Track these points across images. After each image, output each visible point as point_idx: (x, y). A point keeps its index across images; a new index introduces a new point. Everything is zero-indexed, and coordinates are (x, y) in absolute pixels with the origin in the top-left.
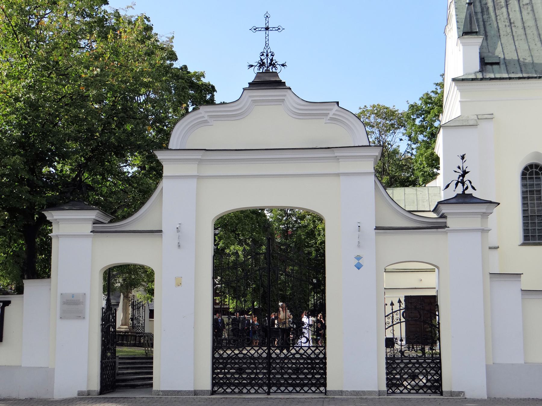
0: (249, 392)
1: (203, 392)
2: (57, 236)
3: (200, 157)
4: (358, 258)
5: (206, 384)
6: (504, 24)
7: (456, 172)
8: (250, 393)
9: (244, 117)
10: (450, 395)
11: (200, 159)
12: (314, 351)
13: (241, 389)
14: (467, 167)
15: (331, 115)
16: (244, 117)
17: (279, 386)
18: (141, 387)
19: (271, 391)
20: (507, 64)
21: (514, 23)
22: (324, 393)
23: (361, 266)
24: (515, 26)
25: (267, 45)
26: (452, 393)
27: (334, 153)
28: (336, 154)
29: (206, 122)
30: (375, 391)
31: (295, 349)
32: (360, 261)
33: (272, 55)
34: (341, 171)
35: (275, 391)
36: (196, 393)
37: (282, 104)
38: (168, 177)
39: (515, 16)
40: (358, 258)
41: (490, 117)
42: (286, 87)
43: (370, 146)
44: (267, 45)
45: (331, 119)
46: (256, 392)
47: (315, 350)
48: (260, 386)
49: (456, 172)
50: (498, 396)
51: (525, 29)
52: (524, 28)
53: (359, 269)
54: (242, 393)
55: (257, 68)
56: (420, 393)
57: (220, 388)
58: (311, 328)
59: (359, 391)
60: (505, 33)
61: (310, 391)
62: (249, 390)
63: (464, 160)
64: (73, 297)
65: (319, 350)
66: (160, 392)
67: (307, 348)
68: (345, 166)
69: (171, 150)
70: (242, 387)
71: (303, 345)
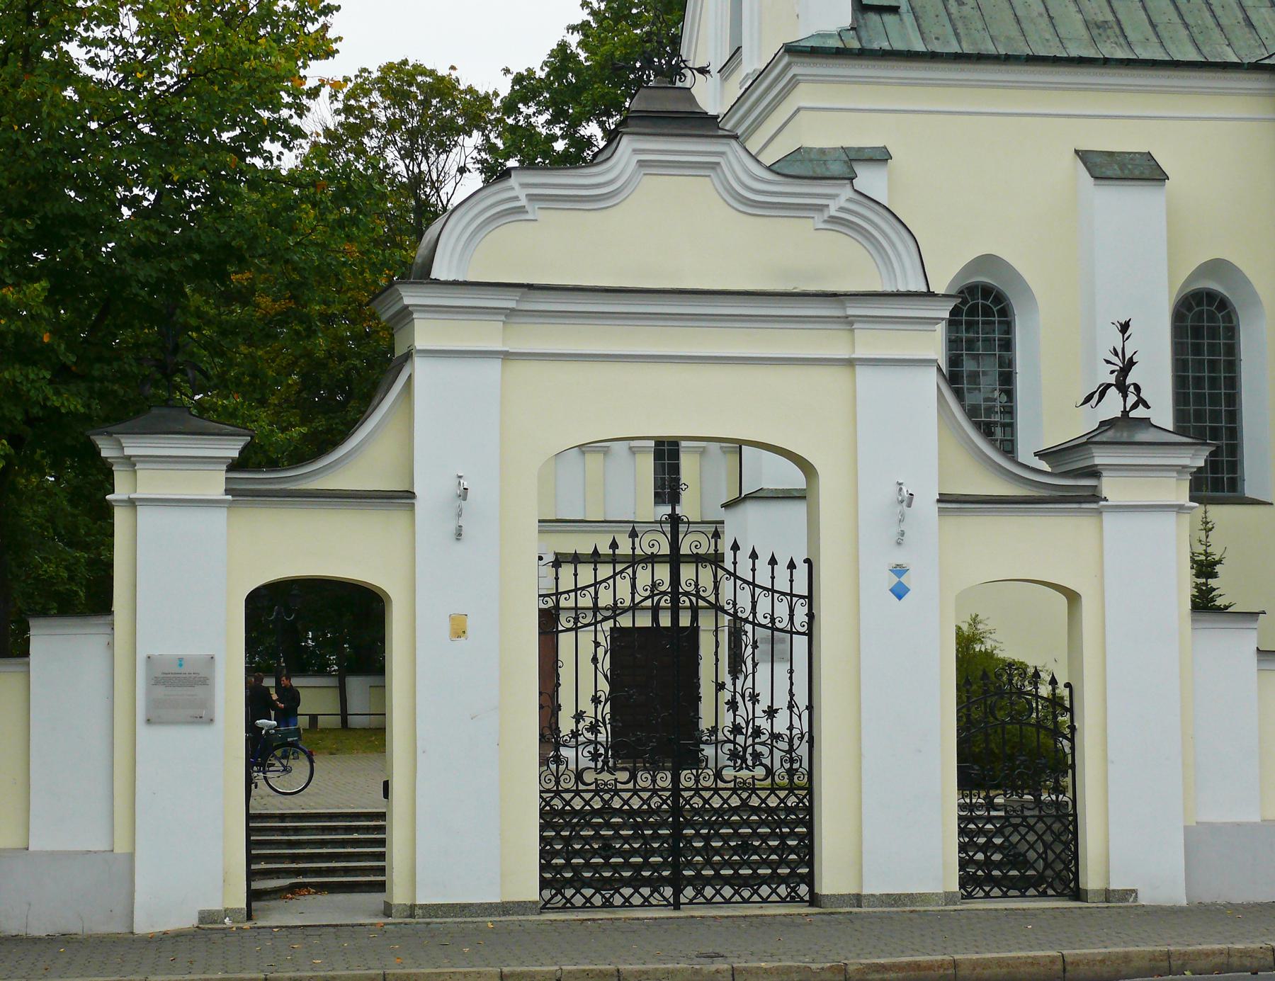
0: (627, 903)
1: (521, 907)
2: (132, 503)
3: (512, 305)
4: (899, 570)
5: (527, 887)
7: (1108, 362)
8: (631, 906)
9: (617, 204)
10: (1103, 898)
11: (513, 310)
12: (648, 799)
13: (607, 896)
14: (1135, 353)
15: (833, 212)
16: (617, 204)
17: (699, 882)
18: (273, 896)
19: (683, 900)
20: (920, 14)
22: (807, 901)
26: (1108, 895)
27: (845, 308)
28: (850, 312)
29: (521, 210)
30: (937, 895)
31: (739, 796)
34: (860, 353)
35: (691, 900)
36: (505, 908)
37: (712, 174)
40: (899, 570)
41: (880, 157)
42: (721, 133)
43: (930, 294)
45: (833, 220)
46: (646, 903)
48: (655, 884)
49: (1108, 362)
50: (1207, 900)
53: (900, 598)
54: (612, 906)
56: (1030, 896)
57: (556, 895)
58: (777, 742)
59: (900, 895)
61: (774, 898)
62: (588, 900)
63: (1126, 336)
64: (181, 665)
65: (660, 797)
66: (416, 908)
67: (630, 794)
68: (869, 343)
69: (437, 282)
70: (612, 892)
71: (620, 786)
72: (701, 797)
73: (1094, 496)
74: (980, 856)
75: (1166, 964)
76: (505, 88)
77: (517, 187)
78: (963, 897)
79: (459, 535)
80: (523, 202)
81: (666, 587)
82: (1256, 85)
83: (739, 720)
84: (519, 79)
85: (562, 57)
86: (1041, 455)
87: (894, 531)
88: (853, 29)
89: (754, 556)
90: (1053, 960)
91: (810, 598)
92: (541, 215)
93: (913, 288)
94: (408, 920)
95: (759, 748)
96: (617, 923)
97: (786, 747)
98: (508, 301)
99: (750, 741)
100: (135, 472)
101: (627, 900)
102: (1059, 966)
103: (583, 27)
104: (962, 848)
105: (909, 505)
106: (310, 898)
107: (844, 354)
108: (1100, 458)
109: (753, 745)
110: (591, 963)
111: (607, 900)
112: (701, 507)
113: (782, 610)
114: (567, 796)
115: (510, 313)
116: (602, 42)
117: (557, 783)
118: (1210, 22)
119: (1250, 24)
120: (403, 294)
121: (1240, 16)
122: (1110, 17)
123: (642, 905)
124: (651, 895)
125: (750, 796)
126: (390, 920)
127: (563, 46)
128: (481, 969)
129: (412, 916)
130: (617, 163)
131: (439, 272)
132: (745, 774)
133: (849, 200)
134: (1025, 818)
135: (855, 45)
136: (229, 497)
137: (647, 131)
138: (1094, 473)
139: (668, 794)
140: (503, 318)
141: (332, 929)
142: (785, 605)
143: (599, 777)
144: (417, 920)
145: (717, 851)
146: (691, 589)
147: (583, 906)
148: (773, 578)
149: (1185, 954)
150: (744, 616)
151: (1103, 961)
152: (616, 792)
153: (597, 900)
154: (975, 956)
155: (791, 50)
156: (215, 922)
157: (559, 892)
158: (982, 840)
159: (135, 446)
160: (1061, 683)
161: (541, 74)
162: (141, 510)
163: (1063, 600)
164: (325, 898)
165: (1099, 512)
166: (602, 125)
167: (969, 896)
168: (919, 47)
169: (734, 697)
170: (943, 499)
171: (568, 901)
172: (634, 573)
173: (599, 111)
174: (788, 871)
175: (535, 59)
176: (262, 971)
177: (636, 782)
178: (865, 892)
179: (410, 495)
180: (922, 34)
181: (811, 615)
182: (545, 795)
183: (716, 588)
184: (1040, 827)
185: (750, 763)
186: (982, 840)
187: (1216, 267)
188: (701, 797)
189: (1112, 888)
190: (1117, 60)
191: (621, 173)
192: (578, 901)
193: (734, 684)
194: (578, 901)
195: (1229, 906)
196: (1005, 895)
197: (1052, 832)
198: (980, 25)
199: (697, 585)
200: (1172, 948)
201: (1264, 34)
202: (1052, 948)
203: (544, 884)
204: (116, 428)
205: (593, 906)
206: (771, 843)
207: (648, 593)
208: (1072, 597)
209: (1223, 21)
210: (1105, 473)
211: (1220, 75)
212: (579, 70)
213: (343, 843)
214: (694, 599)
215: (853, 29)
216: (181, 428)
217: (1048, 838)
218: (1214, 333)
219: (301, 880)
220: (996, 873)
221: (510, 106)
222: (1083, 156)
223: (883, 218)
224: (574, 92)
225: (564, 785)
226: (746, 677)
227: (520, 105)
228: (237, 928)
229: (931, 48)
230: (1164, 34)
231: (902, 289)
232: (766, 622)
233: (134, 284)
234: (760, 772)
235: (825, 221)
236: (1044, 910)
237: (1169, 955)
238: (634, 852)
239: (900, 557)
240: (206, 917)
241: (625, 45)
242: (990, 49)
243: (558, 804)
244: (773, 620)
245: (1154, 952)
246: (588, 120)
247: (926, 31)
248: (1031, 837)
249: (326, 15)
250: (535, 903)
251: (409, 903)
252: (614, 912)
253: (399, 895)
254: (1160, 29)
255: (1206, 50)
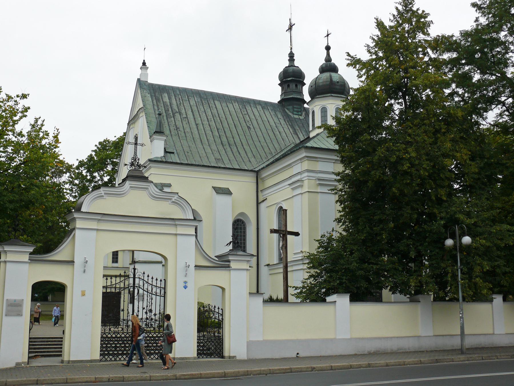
0: (120, 360)
2: (5, 262)
3: (99, 218)
4: (185, 282)
5: (97, 356)
6: (174, 128)
8: (121, 360)
11: (99, 219)
15: (173, 200)
21: (179, 128)
23: (187, 287)
24: (180, 130)
25: (328, 43)
26: (230, 357)
28: (177, 223)
32: (187, 284)
33: (139, 160)
36: (91, 361)
38: (290, 266)
39: (179, 124)
40: (185, 282)
42: (149, 181)
44: (328, 43)
45: (173, 202)
47: (126, 335)
50: (251, 358)
51: (185, 133)
52: (185, 132)
53: (185, 289)
54: (116, 360)
55: (129, 166)
59: (183, 358)
60: (174, 134)
62: (111, 359)
68: (180, 230)
69: (82, 212)
71: (119, 332)
72: (106, 335)
73: (229, 267)
74: (201, 348)
75: (247, 373)
76: (76, 164)
77: (102, 191)
78: (198, 358)
79: (84, 271)
80: (103, 194)
81: (132, 285)
82: (251, 175)
83: (148, 316)
84: (80, 162)
85: (91, 158)
86: (216, 257)
87: (185, 273)
88: (164, 157)
89: (152, 278)
90: (222, 373)
91: (165, 288)
92: (107, 198)
93: (190, 218)
94: (68, 364)
95: (152, 323)
96: (119, 365)
97: (158, 323)
98: (99, 217)
99: (150, 321)
100: (6, 254)
101: (120, 359)
102: (224, 374)
103: (95, 151)
104: (198, 346)
105: (188, 268)
106: (40, 358)
107: (175, 232)
108: (231, 258)
109: (151, 322)
110: (116, 375)
111: (115, 359)
112: (230, 276)
113: (158, 291)
114: (107, 334)
115: (99, 220)
116: (100, 155)
117: (105, 331)
118: (242, 161)
119: (250, 161)
120: (74, 214)
121: (248, 160)
122: (220, 158)
123: (124, 360)
124: (126, 358)
125: (149, 334)
126: (63, 364)
127: (91, 155)
128: (90, 376)
129: (69, 363)
130: (125, 187)
131: (83, 209)
132: (149, 329)
133: (177, 198)
134: (212, 340)
135: (164, 160)
136: (30, 261)
137: (132, 180)
138: (229, 261)
139: (131, 334)
140: (97, 221)
141: (49, 367)
142: (159, 289)
143: (115, 329)
144: (70, 364)
145: (118, 347)
146: (138, 286)
147: (110, 360)
148: (156, 283)
149: (251, 371)
150: (150, 292)
151: (233, 373)
152: (119, 333)
153: (113, 359)
154: (205, 372)
155: (150, 160)
156: (20, 365)
157: (104, 357)
158: (202, 344)
159: (7, 248)
160: (220, 308)
161: (85, 161)
162: (8, 264)
163: (221, 290)
164: (44, 359)
165: (230, 270)
166: (98, 173)
167: (199, 358)
168: (179, 162)
169: (147, 311)
170: (196, 266)
171: (106, 359)
172: (125, 281)
173: (98, 171)
174: (117, 352)
175: (84, 157)
176: (36, 378)
177: (123, 331)
178: (176, 357)
179: (73, 262)
180: (179, 158)
181: (165, 292)
182: (102, 334)
183: (143, 285)
184: (215, 342)
185: (150, 326)
186: (202, 344)
187: (242, 214)
188: (106, 335)
189: (231, 355)
190: (222, 167)
191: (126, 189)
192: (109, 359)
193: (147, 308)
194: (109, 359)
195: (256, 359)
196: (207, 357)
197: (218, 343)
198: (192, 158)
199: (139, 285)
200: (248, 370)
201: (253, 164)
202: (222, 370)
203: (101, 355)
204: (2, 244)
205: (112, 361)
206: (122, 345)
207: (128, 286)
208: (223, 289)
209: (244, 160)
210: (231, 261)
211: (244, 172)
212: (94, 161)
213: (46, 345)
214: (138, 288)
215: (164, 157)
216: (18, 244)
217: (216, 344)
218: (241, 228)
219: (36, 354)
220: (205, 352)
221: (78, 168)
222: (214, 188)
223: (184, 202)
224: (93, 165)
225: (106, 331)
226: (150, 306)
227: (80, 168)
228: (26, 367)
229: (181, 162)
230: (232, 163)
231: (188, 218)
232: (155, 293)
233: (8, 209)
234: (152, 329)
235: (171, 202)
236: (216, 361)
237: (248, 371)
238: (109, 347)
239: (186, 279)
240: (17, 364)
241: (106, 156)
242: (194, 163)
243: (105, 336)
244: (156, 293)
245: (244, 371)
246: (95, 172)
247: (180, 158)
248: (213, 344)
249: (56, 148)
250: (98, 360)
251: (68, 360)
252: (117, 362)
253: (66, 358)
254: (231, 161)
255: (241, 166)
